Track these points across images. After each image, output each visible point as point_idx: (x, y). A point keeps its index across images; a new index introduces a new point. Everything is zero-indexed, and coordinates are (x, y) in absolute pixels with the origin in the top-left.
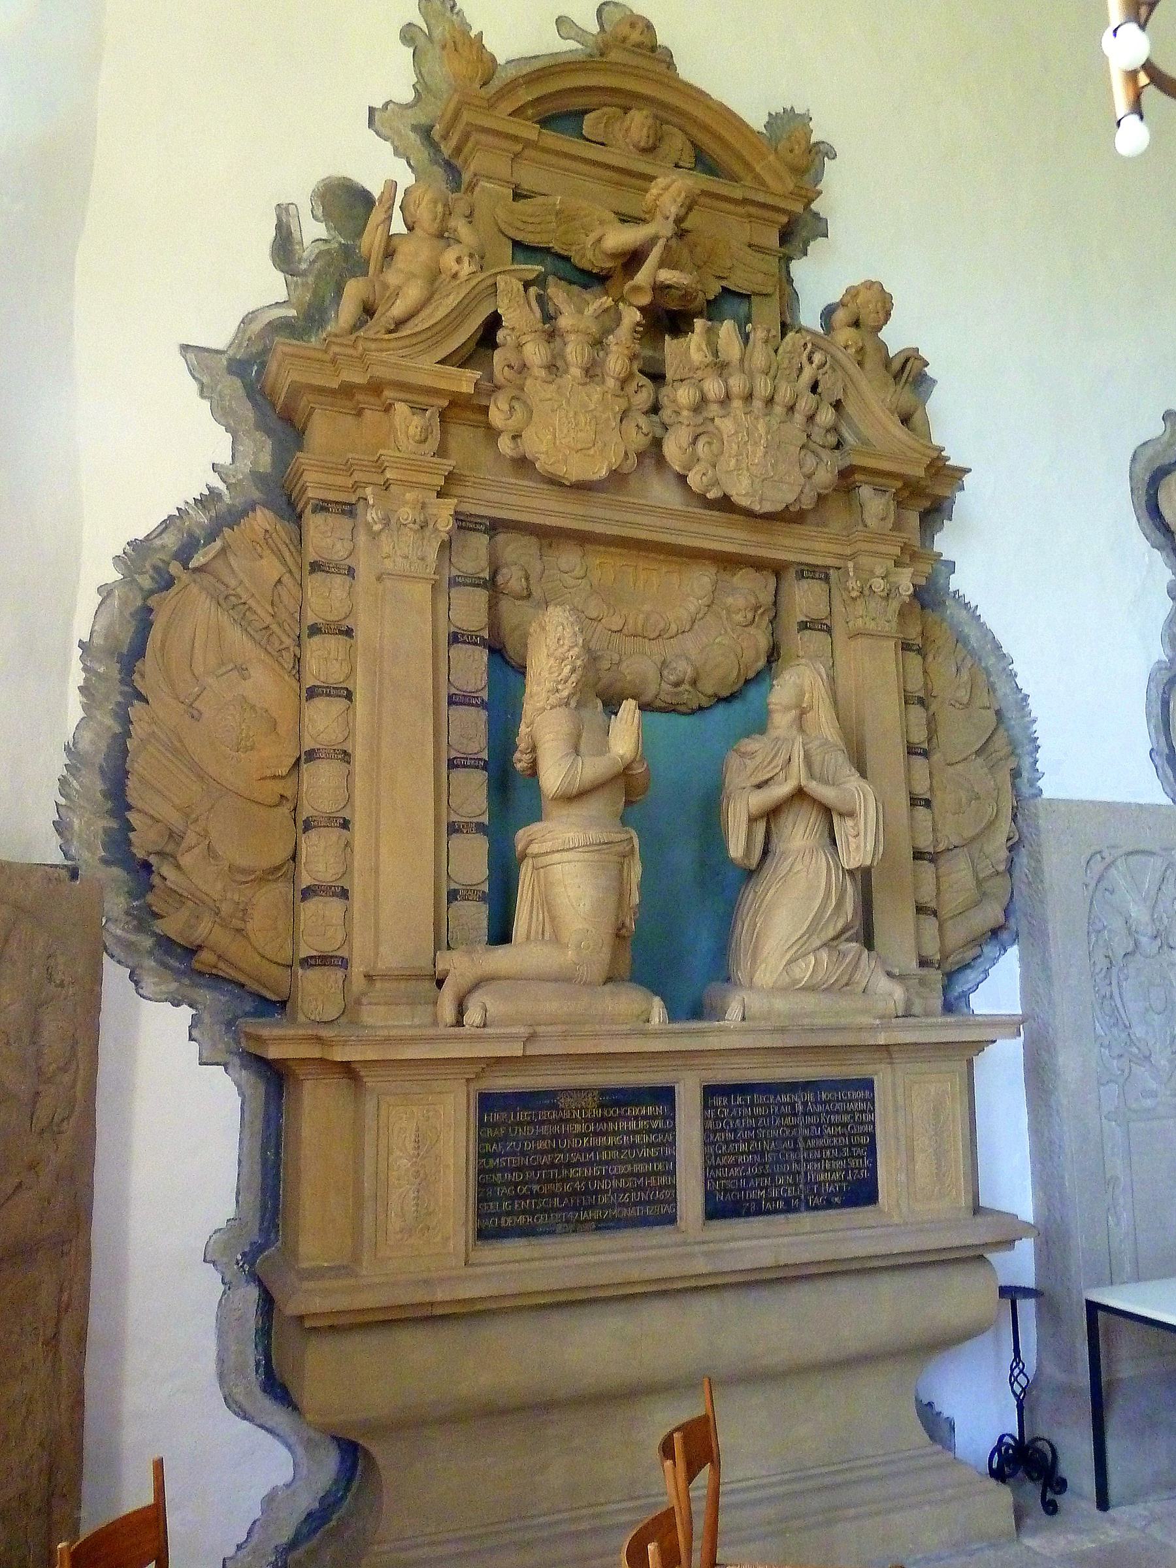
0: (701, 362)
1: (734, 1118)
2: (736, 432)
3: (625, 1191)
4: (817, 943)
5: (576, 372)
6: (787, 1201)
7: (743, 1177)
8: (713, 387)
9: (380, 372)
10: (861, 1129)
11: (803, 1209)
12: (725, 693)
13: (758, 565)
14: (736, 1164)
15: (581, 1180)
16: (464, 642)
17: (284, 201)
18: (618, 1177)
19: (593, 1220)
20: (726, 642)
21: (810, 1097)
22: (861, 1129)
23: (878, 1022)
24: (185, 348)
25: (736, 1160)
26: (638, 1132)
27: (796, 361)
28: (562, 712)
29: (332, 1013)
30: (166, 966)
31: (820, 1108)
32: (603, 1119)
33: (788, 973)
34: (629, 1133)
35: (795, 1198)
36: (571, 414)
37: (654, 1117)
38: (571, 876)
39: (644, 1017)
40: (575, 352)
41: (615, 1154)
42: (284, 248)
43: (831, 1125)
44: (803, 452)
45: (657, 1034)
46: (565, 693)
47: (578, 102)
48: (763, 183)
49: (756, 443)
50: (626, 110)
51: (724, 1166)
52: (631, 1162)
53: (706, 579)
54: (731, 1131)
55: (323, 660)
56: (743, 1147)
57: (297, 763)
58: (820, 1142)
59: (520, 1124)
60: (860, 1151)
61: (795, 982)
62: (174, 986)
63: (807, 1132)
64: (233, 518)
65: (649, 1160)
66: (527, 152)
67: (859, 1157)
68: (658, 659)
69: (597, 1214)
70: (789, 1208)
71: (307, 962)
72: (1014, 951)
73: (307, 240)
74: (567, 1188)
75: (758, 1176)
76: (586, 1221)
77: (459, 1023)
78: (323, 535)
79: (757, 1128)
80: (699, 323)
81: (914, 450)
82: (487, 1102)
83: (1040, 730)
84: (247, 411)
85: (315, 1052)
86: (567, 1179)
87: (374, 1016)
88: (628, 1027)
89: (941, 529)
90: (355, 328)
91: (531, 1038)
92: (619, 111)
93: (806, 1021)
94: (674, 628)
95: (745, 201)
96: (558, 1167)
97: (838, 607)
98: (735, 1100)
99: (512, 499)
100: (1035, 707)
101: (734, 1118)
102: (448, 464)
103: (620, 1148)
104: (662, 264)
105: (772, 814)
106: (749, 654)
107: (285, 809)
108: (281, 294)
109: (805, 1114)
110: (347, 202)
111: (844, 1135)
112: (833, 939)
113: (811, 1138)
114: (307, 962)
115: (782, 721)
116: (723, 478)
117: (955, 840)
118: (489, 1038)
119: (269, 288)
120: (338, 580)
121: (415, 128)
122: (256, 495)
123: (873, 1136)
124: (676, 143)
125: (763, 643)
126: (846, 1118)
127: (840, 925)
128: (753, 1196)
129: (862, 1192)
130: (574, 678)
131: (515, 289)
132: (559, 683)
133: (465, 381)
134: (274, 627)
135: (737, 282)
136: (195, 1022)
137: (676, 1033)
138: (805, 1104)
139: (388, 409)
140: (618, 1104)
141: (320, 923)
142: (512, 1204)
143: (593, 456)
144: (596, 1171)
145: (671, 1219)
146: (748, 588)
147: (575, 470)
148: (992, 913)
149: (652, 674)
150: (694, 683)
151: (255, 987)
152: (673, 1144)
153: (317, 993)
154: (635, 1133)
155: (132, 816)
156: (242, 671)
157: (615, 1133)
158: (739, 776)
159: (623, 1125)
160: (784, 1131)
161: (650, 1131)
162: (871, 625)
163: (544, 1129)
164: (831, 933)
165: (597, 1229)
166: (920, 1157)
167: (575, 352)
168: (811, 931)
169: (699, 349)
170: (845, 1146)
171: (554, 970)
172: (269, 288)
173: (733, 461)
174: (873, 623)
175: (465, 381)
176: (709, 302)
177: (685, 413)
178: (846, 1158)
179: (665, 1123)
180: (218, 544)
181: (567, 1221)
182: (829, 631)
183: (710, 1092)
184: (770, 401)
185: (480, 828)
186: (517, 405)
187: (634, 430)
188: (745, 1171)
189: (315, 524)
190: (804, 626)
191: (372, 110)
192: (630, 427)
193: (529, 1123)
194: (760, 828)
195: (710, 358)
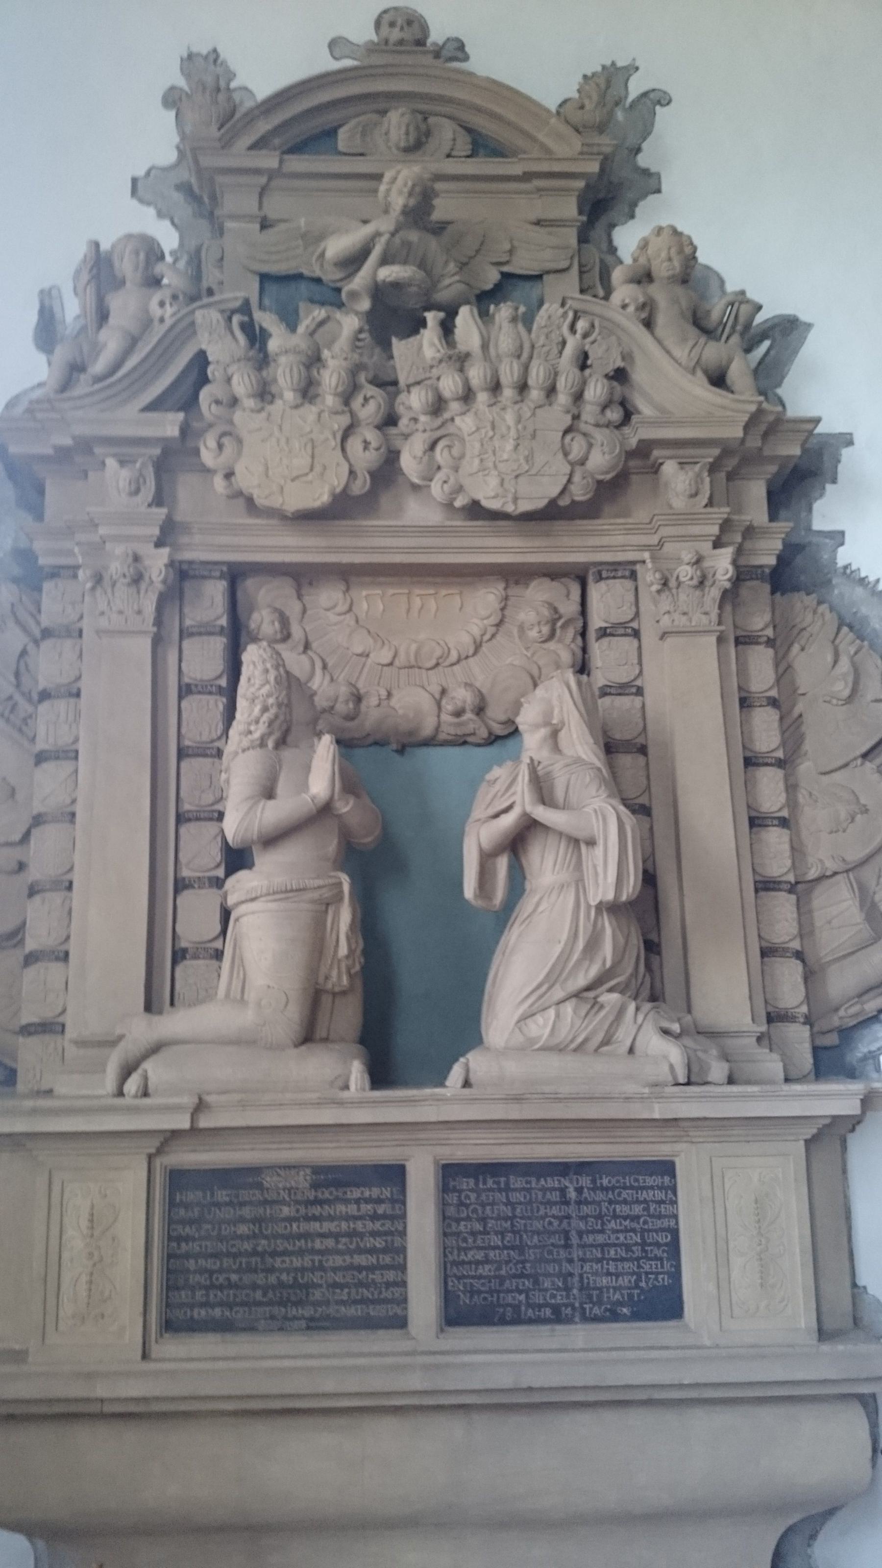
0: (433, 358)
1: (483, 1205)
2: (478, 429)
3: (342, 1286)
4: (558, 993)
5: (289, 396)
6: (556, 1309)
7: (495, 1277)
8: (449, 384)
9: (80, 430)
10: (659, 1224)
11: (577, 1319)
13: (553, 573)
14: (487, 1261)
15: (288, 1271)
16: (199, 693)
17: (46, 285)
18: (335, 1270)
19: (303, 1317)
20: (516, 663)
21: (585, 1181)
22: (659, 1224)
23: (646, 1090)
25: (486, 1256)
26: (360, 1218)
27: (555, 337)
28: (254, 755)
31: (600, 1196)
32: (317, 1202)
33: (537, 1033)
34: (348, 1218)
35: (566, 1306)
36: (283, 441)
37: (379, 1201)
38: (267, 935)
39: (340, 1083)
40: (285, 375)
41: (330, 1243)
42: (47, 332)
43: (615, 1216)
44: (568, 438)
45: (360, 1103)
46: (257, 735)
47: (332, 117)
48: (547, 150)
49: (503, 437)
50: (383, 113)
51: (470, 1263)
52: (351, 1253)
53: (491, 597)
54: (478, 1220)
56: (496, 1240)
58: (600, 1239)
59: (218, 1205)
60: (658, 1252)
61: (532, 1041)
63: (582, 1226)
65: (372, 1251)
66: (273, 184)
67: (656, 1258)
68: (436, 690)
69: (308, 1312)
70: (558, 1317)
71: (27, 1030)
74: (272, 1279)
75: (515, 1276)
76: (295, 1318)
77: (120, 1093)
79: (515, 1216)
81: (724, 408)
82: (178, 1179)
86: (271, 1270)
88: (317, 1095)
89: (821, 496)
91: (200, 1107)
92: (374, 117)
93: (547, 1089)
94: (454, 656)
95: (527, 177)
96: (262, 1255)
98: (485, 1183)
99: (244, 541)
101: (483, 1205)
103: (337, 1236)
104: (385, 261)
105: (517, 843)
109: (579, 1203)
111: (633, 1230)
112: (588, 989)
113: (588, 1232)
114: (27, 1030)
116: (466, 482)
117: (831, 866)
118: (151, 1110)
120: (68, 643)
121: (179, 187)
123: (675, 1233)
124: (446, 133)
126: (637, 1209)
127: (594, 971)
128: (509, 1299)
129: (664, 1304)
130: (266, 717)
131: (214, 322)
132: (249, 724)
134: (18, 697)
135: (521, 265)
137: (375, 1102)
138: (579, 1190)
139: (656, 469)
140: (338, 1184)
142: (207, 1295)
143: (311, 482)
144: (307, 1261)
145: (401, 1323)
146: (538, 596)
149: (426, 703)
150: (480, 710)
152: (403, 1234)
154: (356, 1218)
157: (331, 1218)
159: (341, 1208)
160: (550, 1223)
161: (375, 1217)
162: (681, 622)
163: (246, 1212)
164: (581, 980)
165: (308, 1328)
166: (737, 1262)
167: (285, 375)
168: (552, 979)
169: (432, 344)
170: (636, 1244)
173: (477, 461)
174: (684, 619)
175: (169, 425)
177: (423, 418)
178: (638, 1259)
179: (393, 1208)
181: (272, 1317)
182: (636, 634)
183: (450, 1173)
184: (523, 387)
187: (360, 447)
188: (499, 1268)
190: (603, 633)
191: (134, 181)
192: (355, 445)
193: (227, 1204)
194: (502, 863)
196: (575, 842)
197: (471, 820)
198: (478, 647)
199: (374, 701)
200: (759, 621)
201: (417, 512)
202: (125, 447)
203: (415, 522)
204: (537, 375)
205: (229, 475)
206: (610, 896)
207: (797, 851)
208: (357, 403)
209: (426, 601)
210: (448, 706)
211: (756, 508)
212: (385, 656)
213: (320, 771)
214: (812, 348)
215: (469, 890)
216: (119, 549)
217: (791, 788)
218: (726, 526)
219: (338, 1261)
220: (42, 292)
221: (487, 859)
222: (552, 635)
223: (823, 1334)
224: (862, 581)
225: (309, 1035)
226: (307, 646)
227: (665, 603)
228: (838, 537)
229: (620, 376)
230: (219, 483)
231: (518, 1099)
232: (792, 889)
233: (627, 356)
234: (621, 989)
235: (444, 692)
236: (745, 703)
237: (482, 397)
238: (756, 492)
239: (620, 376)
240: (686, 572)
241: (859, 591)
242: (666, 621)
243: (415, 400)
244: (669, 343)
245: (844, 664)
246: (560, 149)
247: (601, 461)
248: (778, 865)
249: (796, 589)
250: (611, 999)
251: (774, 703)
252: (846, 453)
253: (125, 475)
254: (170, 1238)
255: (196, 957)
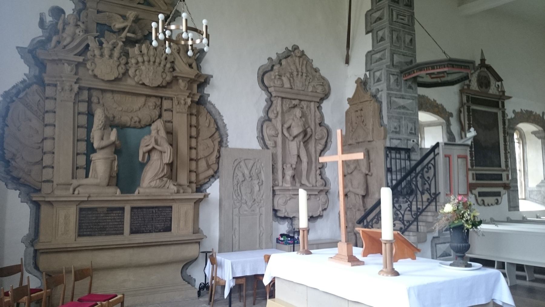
4: (156, 178)
5: (107, 56)
8: (140, 59)
9: (60, 57)
12: (148, 124)
17: (42, 12)
21: (157, 210)
24: (17, 48)
29: (49, 192)
30: (13, 182)
33: (151, 183)
38: (100, 164)
40: (106, 52)
42: (42, 23)
55: (49, 119)
57: (43, 140)
62: (15, 186)
64: (28, 86)
69: (105, 232)
70: (150, 232)
71: (44, 182)
72: (218, 180)
73: (47, 21)
77: (73, 193)
78: (49, 91)
80: (137, 45)
82: (81, 210)
83: (229, 132)
84: (32, 61)
85: (43, 199)
87: (58, 192)
90: (55, 47)
91: (89, 197)
94: (135, 110)
97: (174, 106)
100: (228, 127)
102: (77, 77)
103: (111, 219)
104: (128, 32)
105: (149, 152)
106: (154, 116)
107: (41, 150)
108: (41, 34)
110: (58, 12)
114: (44, 182)
115: (154, 133)
117: (202, 156)
119: (38, 33)
122: (35, 81)
123: (171, 218)
125: (157, 113)
127: (163, 174)
129: (168, 229)
133: (81, 59)
136: (20, 194)
140: (111, 210)
141: (47, 174)
145: (122, 234)
146: (152, 102)
147: (107, 78)
148: (211, 172)
149: (129, 119)
150: (140, 122)
151: (33, 187)
152: (124, 219)
153: (46, 188)
155: (5, 151)
156: (30, 120)
158: (143, 144)
159: (112, 215)
161: (118, 216)
162: (181, 111)
164: (160, 176)
166: (181, 222)
167: (106, 52)
171: (97, 184)
172: (38, 33)
175: (81, 59)
176: (145, 36)
180: (25, 92)
182: (172, 111)
184: (154, 62)
185: (84, 154)
186: (93, 64)
189: (47, 88)
190: (166, 110)
192: (120, 68)
194: (147, 155)
195: (140, 53)
196: (161, 152)
197: (140, 147)
198: (140, 109)
199: (117, 118)
200: (194, 111)
201: (130, 81)
202: (70, 62)
203: (129, 83)
204: (158, 60)
205: (93, 71)
206: (168, 162)
207: (197, 153)
208: (121, 59)
209: (129, 98)
210: (133, 121)
211: (195, 90)
212: (120, 109)
213: (113, 136)
214: (207, 57)
215: (140, 159)
216: (68, 84)
217: (197, 142)
218: (190, 94)
219: (111, 223)
220: (40, 13)
221: (144, 154)
222: (155, 108)
223: (194, 233)
224: (212, 104)
225: (108, 185)
226: (103, 105)
227: (178, 107)
228: (209, 95)
229: (173, 62)
230: (90, 72)
231: (147, 196)
232: (195, 160)
233: (174, 59)
234: (167, 177)
235: (132, 117)
236: (191, 126)
237: (146, 63)
238: (195, 86)
239: (173, 62)
240: (183, 102)
241: (211, 106)
242: (178, 110)
243: (133, 61)
244: (182, 58)
245: (208, 120)
246: (163, 8)
247: (168, 78)
248: (194, 156)
249: (201, 104)
250: (165, 179)
251: (195, 127)
252: (211, 79)
253: (69, 68)
254: (79, 220)
255: (80, 168)
